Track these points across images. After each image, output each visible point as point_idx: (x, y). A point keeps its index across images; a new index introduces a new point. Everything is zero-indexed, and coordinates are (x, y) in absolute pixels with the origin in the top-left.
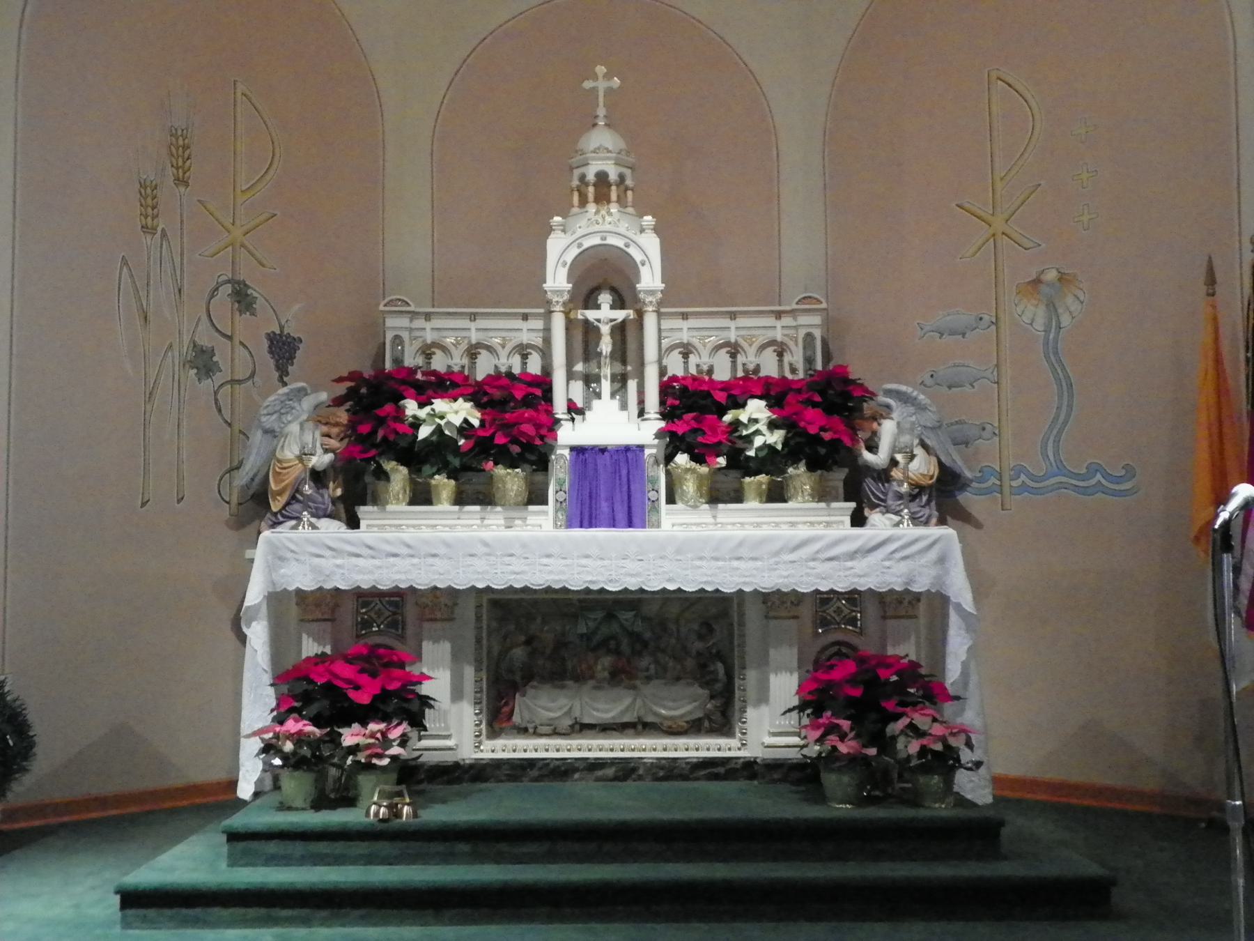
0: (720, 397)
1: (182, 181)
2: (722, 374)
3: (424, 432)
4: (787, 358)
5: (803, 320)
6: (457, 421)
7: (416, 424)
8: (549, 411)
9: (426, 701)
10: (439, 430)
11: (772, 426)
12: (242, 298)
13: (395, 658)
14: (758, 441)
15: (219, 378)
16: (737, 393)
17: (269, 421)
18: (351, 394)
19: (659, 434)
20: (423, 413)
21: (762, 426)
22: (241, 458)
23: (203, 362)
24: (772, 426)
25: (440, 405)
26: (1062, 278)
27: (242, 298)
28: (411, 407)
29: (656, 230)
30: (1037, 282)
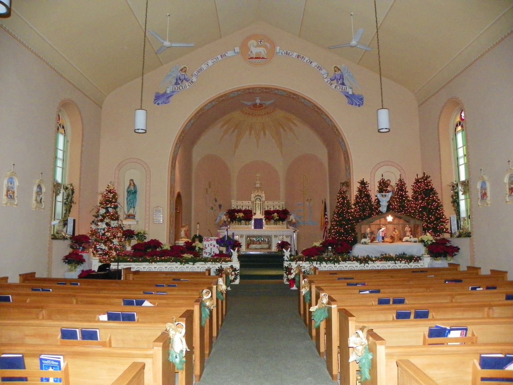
0: (272, 213)
1: (210, 188)
2: (272, 210)
3: (238, 217)
4: (280, 207)
5: (282, 202)
6: (242, 216)
7: (237, 216)
8: (252, 214)
9: (241, 245)
10: (239, 217)
11: (277, 216)
12: (216, 200)
13: (458, 201)
14: (276, 218)
15: (214, 210)
16: (274, 212)
17: (220, 215)
18: (229, 212)
19: (264, 217)
20: (238, 215)
21: (276, 216)
22: (314, 281)
23: (212, 208)
24: (277, 216)
25: (240, 214)
26: (311, 200)
27: (216, 200)
28: (236, 214)
29: (264, 193)
30: (308, 200)
